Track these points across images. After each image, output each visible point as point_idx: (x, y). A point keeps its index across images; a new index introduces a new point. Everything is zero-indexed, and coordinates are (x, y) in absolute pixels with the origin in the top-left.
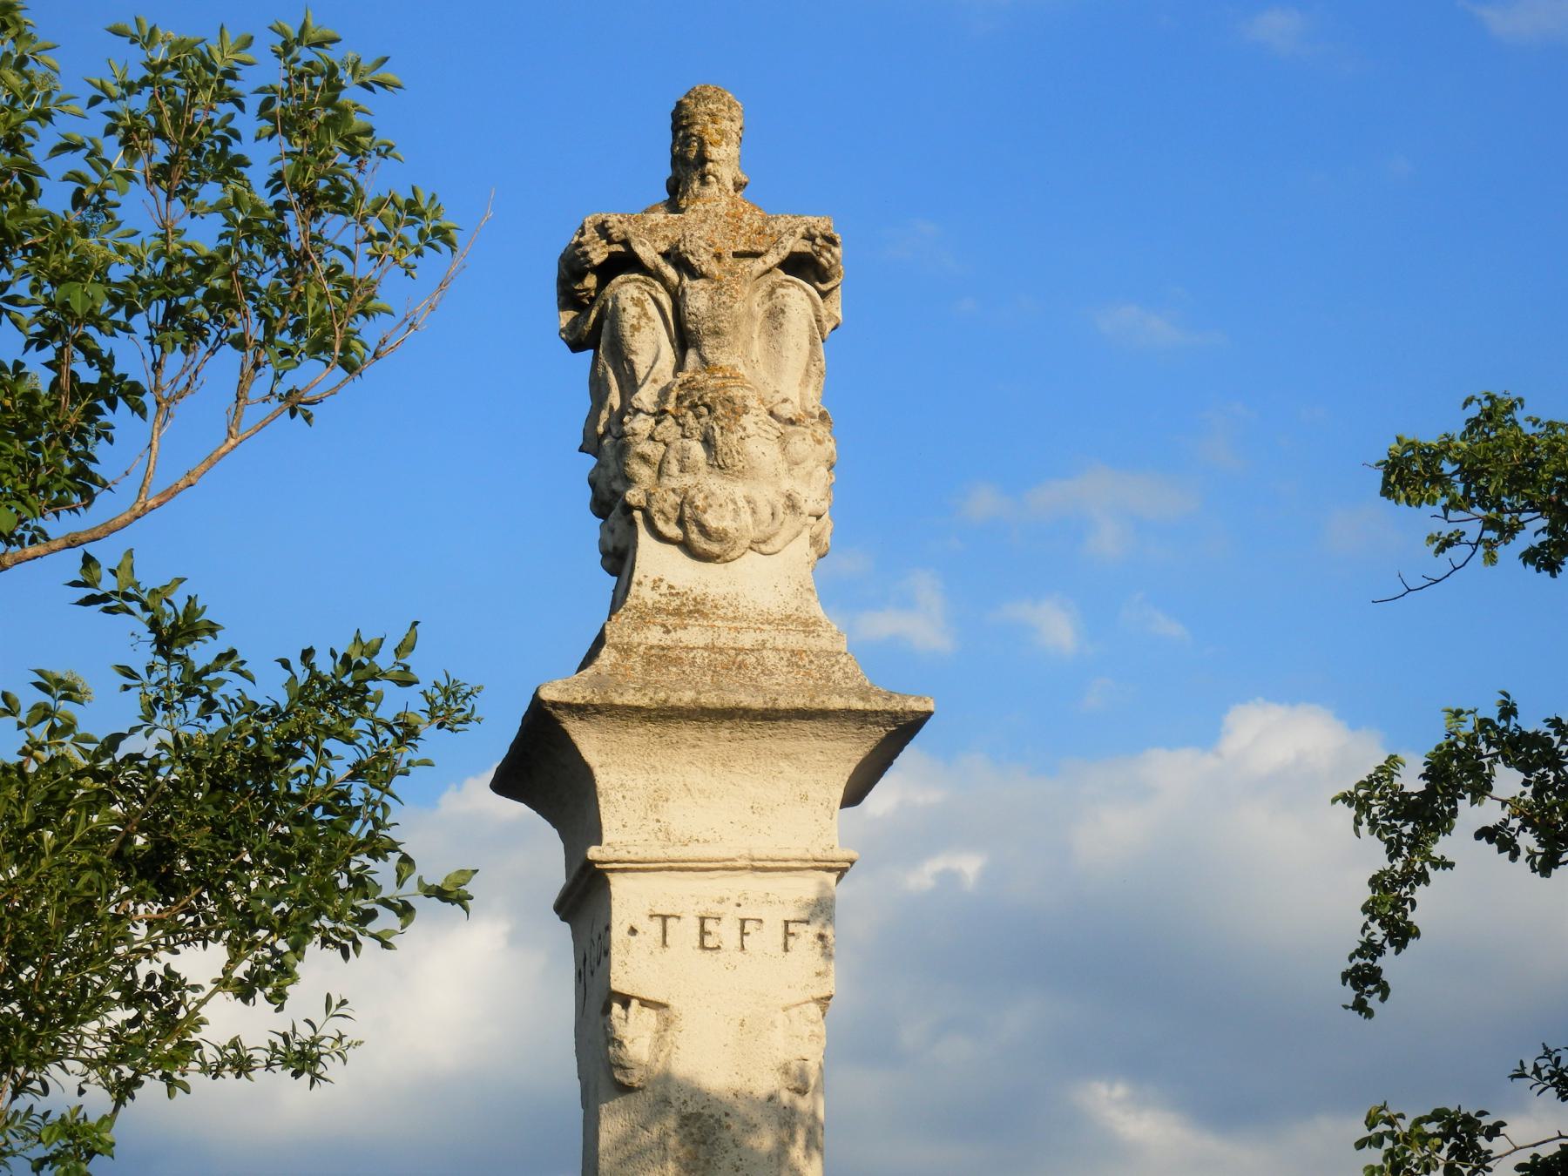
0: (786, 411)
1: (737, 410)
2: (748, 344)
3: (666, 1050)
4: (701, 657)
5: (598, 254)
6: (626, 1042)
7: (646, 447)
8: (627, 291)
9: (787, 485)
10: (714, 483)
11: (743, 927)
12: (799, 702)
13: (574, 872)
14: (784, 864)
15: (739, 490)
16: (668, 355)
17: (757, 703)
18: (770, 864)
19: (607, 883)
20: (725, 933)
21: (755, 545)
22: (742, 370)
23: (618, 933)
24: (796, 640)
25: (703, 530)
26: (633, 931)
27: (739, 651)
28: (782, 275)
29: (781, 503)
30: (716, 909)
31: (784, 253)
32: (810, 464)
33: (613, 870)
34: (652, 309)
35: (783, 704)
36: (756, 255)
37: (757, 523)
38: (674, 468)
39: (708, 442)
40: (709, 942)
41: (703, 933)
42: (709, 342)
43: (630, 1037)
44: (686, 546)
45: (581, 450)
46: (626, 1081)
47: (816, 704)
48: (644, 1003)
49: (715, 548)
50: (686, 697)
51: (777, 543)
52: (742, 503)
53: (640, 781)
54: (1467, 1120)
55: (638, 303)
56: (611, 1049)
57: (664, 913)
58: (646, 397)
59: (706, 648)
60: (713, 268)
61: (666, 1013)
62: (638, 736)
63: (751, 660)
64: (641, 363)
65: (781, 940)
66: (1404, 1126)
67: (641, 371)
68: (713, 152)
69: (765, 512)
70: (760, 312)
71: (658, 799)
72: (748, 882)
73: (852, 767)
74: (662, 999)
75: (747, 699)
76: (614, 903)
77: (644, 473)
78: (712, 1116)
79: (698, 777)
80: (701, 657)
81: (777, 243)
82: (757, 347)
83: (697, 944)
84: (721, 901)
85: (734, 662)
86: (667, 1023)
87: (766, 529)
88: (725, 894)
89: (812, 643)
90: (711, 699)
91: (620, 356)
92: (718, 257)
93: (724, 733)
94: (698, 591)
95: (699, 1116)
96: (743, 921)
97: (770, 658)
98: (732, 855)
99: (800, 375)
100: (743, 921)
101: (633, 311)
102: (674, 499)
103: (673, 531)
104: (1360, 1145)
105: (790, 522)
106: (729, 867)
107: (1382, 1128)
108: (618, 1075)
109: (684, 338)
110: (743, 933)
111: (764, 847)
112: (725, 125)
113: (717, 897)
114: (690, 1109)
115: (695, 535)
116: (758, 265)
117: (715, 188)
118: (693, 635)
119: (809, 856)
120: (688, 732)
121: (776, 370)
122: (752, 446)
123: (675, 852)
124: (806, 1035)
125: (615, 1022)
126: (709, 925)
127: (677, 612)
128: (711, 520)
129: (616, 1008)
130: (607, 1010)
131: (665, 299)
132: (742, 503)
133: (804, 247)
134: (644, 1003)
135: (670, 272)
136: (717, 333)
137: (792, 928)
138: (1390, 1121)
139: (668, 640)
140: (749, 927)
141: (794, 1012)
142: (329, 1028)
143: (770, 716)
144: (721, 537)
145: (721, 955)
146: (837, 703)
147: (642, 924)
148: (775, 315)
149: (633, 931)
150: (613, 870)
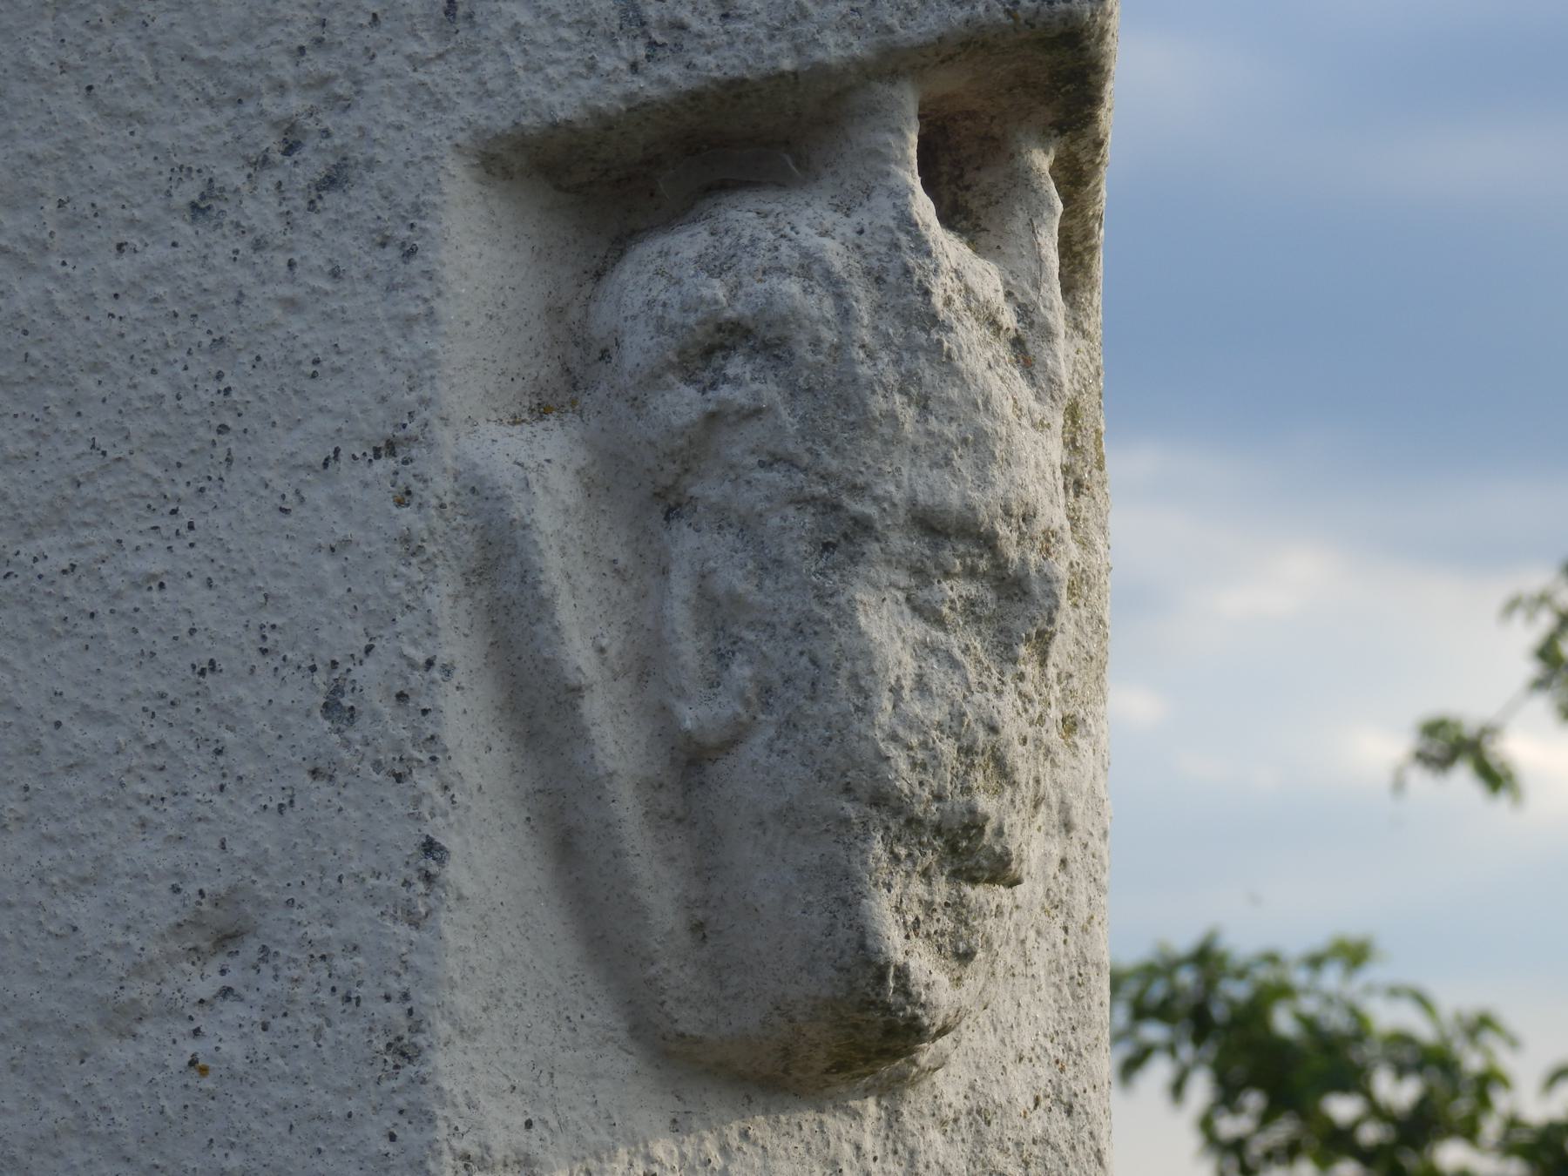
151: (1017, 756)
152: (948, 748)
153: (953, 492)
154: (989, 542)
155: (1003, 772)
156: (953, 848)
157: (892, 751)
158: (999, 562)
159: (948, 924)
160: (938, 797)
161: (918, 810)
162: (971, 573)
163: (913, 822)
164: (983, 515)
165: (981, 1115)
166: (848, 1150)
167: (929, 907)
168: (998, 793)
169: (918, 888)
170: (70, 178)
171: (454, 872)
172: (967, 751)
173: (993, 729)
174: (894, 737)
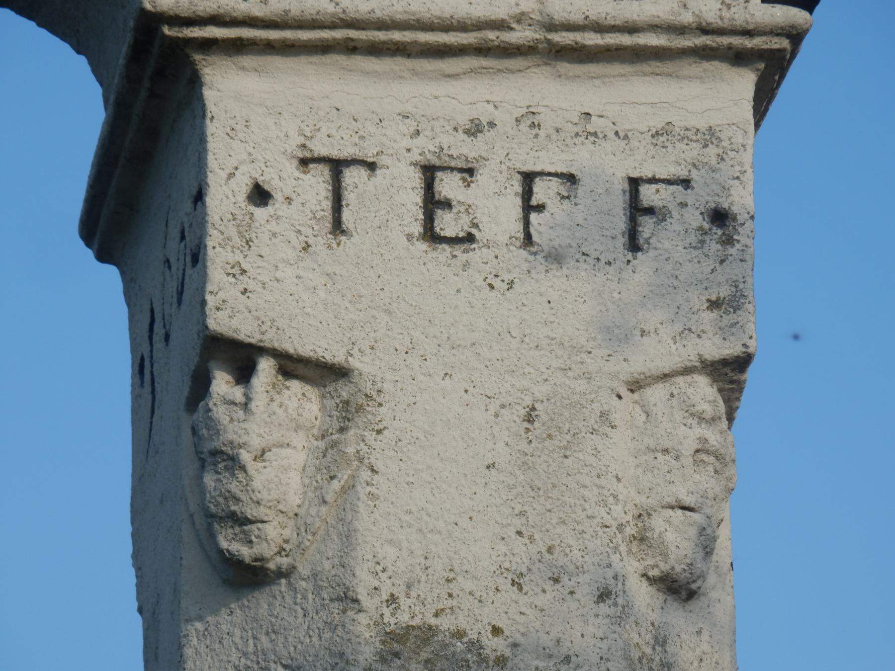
3: (344, 476)
6: (245, 456)
11: (527, 194)
13: (112, 98)
14: (626, 40)
18: (591, 39)
19: (195, 82)
20: (490, 204)
23: (224, 198)
26: (260, 195)
30: (464, 148)
33: (208, 45)
40: (448, 224)
41: (432, 203)
43: (256, 443)
46: (245, 552)
48: (292, 366)
56: (209, 480)
57: (335, 154)
61: (345, 390)
65: (621, 223)
72: (557, 93)
74: (334, 354)
76: (211, 128)
78: (459, 634)
83: (417, 229)
84: (475, 130)
86: (347, 413)
88: (485, 113)
95: (428, 633)
96: (528, 178)
98: (500, 12)
100: (528, 178)
108: (228, 542)
110: (529, 207)
113: (463, 121)
114: (404, 618)
119: (687, 18)
124: (689, 446)
125: (220, 412)
126: (448, 186)
129: (222, 384)
130: (200, 386)
134: (292, 366)
137: (649, 195)
140: (542, 191)
141: (656, 394)
145: (477, 255)
147: (283, 177)
149: (260, 195)
150: (208, 45)
151: (239, 494)
152: (221, 500)
153: (216, 444)
154: (222, 452)
155: (238, 500)
156: (233, 519)
157: (209, 505)
158: (228, 455)
159: (242, 536)
160: (223, 511)
161: (220, 515)
162: (224, 460)
163: (221, 518)
164: (218, 448)
165: (315, 575)
166: (277, 592)
167: (235, 534)
168: (238, 504)
169: (230, 531)
170: (580, 455)
171: (184, 562)
172: (226, 498)
173: (229, 492)
174: (210, 502)
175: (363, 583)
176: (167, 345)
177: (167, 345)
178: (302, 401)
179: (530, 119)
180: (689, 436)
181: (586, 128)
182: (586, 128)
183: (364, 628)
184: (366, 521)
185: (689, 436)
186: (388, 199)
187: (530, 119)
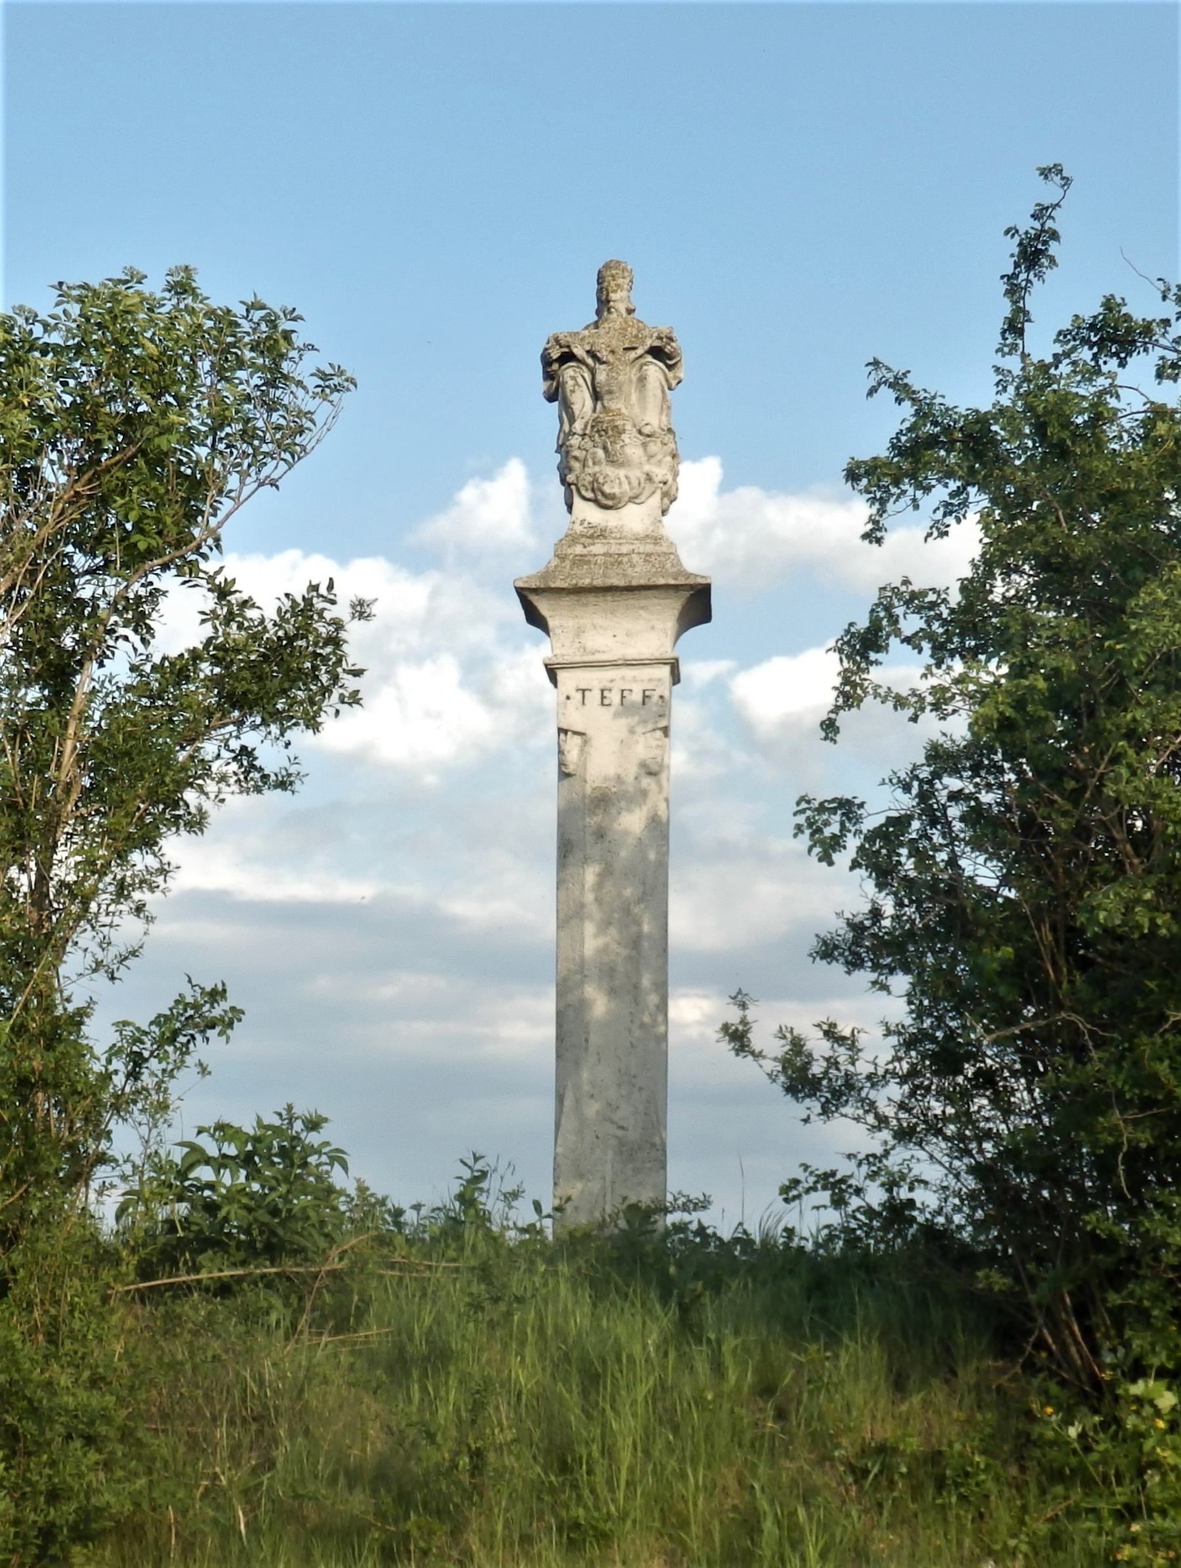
0: (647, 430)
1: (619, 432)
2: (629, 395)
4: (600, 560)
5: (555, 354)
7: (576, 453)
8: (569, 372)
9: (647, 468)
10: (609, 471)
12: (643, 582)
15: (622, 473)
16: (589, 403)
17: (622, 583)
21: (633, 499)
22: (624, 411)
24: (650, 548)
25: (603, 494)
26: (568, 698)
27: (620, 555)
28: (649, 358)
29: (643, 477)
30: (609, 685)
31: (646, 347)
32: (659, 457)
34: (580, 381)
35: (634, 583)
36: (634, 349)
37: (632, 489)
38: (590, 463)
39: (605, 448)
40: (606, 702)
41: (603, 697)
42: (607, 397)
44: (595, 501)
45: (1077, 316)
47: (651, 583)
48: (575, 733)
49: (610, 503)
50: (586, 582)
51: (642, 498)
52: (623, 479)
53: (571, 623)
54: (848, 801)
55: (573, 378)
58: (578, 426)
59: (605, 555)
60: (611, 358)
62: (566, 601)
63: (625, 559)
64: (576, 408)
66: (816, 804)
67: (577, 413)
68: (613, 296)
69: (635, 483)
70: (634, 378)
71: (579, 632)
72: (628, 672)
73: (676, 613)
75: (616, 581)
77: (576, 465)
79: (599, 620)
80: (600, 560)
81: (643, 343)
82: (634, 397)
85: (616, 560)
86: (585, 743)
87: (636, 491)
89: (658, 549)
90: (598, 582)
91: (566, 406)
92: (613, 352)
93: (609, 598)
94: (603, 524)
97: (635, 558)
99: (658, 410)
101: (571, 382)
102: (590, 479)
103: (590, 495)
104: (795, 814)
105: (649, 488)
106: (614, 664)
107: (804, 805)
109: (596, 396)
111: (632, 653)
112: (620, 281)
115: (600, 497)
116: (633, 355)
117: (615, 315)
118: (598, 548)
120: (591, 598)
121: (644, 408)
122: (629, 450)
123: (586, 659)
126: (606, 693)
127: (591, 537)
128: (607, 489)
131: (587, 376)
132: (623, 479)
133: (657, 343)
134: (575, 733)
135: (590, 361)
136: (610, 392)
138: (808, 802)
139: (585, 551)
142: (293, 769)
143: (630, 589)
144: (612, 497)
146: (662, 581)
148: (642, 380)
149: (568, 698)
175: (588, 778)
176: (827, 951)
177: (827, 951)
178: (577, 740)
179: (623, 678)
180: (655, 743)
181: (635, 680)
182: (635, 680)
183: (589, 790)
184: (589, 766)
185: (655, 743)
186: (594, 697)
187: (623, 678)
